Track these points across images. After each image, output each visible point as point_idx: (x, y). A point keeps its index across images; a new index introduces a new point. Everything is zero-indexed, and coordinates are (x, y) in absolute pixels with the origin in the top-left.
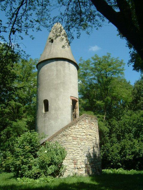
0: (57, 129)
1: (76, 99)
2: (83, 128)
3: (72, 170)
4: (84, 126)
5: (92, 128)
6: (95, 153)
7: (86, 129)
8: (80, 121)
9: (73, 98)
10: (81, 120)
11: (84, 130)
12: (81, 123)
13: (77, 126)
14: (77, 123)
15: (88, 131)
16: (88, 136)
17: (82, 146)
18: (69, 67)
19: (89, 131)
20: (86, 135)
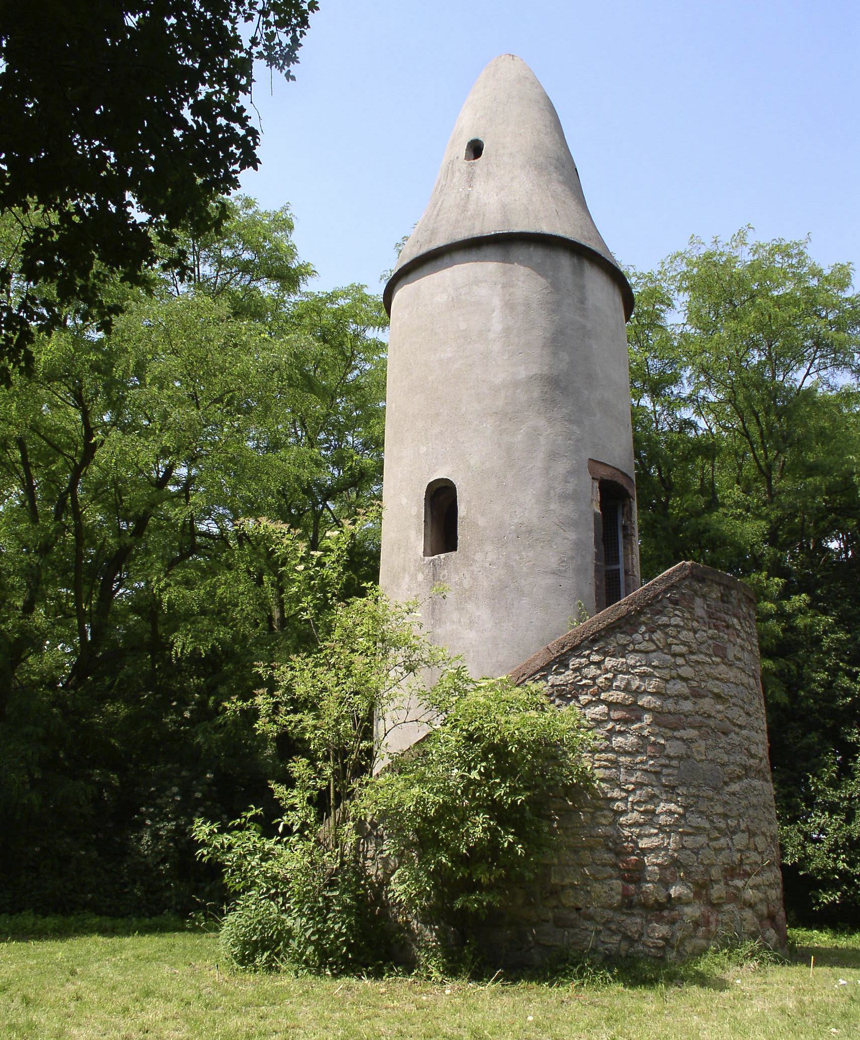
0: (611, 470)
1: (621, 481)
2: (676, 649)
3: (609, 914)
4: (685, 635)
5: (731, 657)
6: (42, 207)
7: (694, 657)
8: (658, 607)
9: (604, 473)
10: (665, 602)
11: (680, 661)
12: (664, 620)
13: (637, 637)
14: (643, 619)
15: (708, 669)
16: (707, 704)
17: (674, 763)
18: (582, 288)
19: (715, 672)
20: (696, 694)
